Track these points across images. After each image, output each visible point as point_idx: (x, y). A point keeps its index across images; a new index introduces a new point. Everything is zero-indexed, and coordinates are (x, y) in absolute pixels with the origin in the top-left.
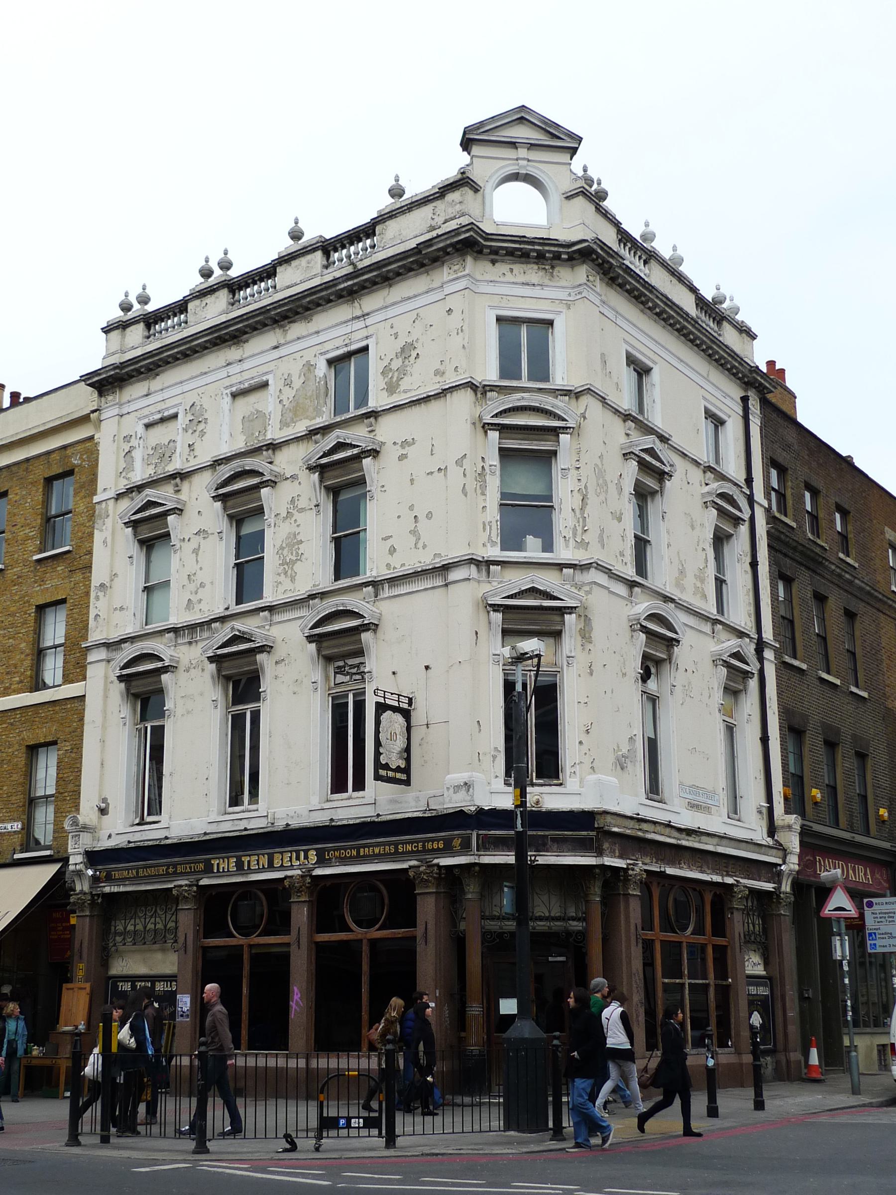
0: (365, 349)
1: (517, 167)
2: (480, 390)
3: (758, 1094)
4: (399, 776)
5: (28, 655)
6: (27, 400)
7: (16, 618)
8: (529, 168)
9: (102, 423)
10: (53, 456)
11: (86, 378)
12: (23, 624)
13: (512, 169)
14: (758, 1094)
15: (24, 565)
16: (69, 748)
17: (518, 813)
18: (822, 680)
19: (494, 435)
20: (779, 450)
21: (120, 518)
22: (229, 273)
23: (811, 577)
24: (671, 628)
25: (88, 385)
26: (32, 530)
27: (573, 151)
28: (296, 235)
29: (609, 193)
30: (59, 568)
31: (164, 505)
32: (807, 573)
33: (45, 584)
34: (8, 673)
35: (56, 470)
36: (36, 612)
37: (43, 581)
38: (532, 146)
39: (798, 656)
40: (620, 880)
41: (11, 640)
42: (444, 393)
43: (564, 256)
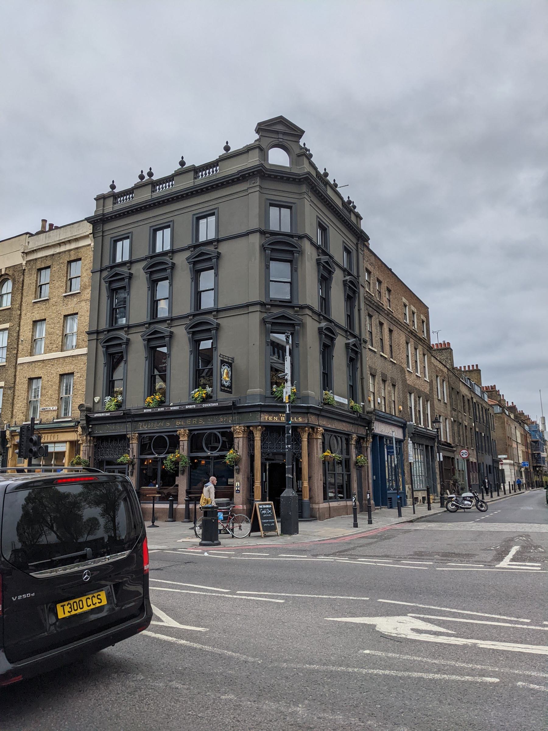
3: (370, 517)
4: (228, 389)
5: (60, 336)
6: (57, 228)
11: (87, 219)
13: (276, 142)
14: (370, 517)
17: (288, 406)
18: (381, 356)
20: (369, 265)
22: (114, 190)
23: (378, 315)
24: (334, 334)
27: (300, 136)
28: (182, 163)
31: (123, 275)
32: (377, 314)
34: (51, 343)
35: (72, 258)
36: (64, 318)
38: (284, 134)
39: (374, 346)
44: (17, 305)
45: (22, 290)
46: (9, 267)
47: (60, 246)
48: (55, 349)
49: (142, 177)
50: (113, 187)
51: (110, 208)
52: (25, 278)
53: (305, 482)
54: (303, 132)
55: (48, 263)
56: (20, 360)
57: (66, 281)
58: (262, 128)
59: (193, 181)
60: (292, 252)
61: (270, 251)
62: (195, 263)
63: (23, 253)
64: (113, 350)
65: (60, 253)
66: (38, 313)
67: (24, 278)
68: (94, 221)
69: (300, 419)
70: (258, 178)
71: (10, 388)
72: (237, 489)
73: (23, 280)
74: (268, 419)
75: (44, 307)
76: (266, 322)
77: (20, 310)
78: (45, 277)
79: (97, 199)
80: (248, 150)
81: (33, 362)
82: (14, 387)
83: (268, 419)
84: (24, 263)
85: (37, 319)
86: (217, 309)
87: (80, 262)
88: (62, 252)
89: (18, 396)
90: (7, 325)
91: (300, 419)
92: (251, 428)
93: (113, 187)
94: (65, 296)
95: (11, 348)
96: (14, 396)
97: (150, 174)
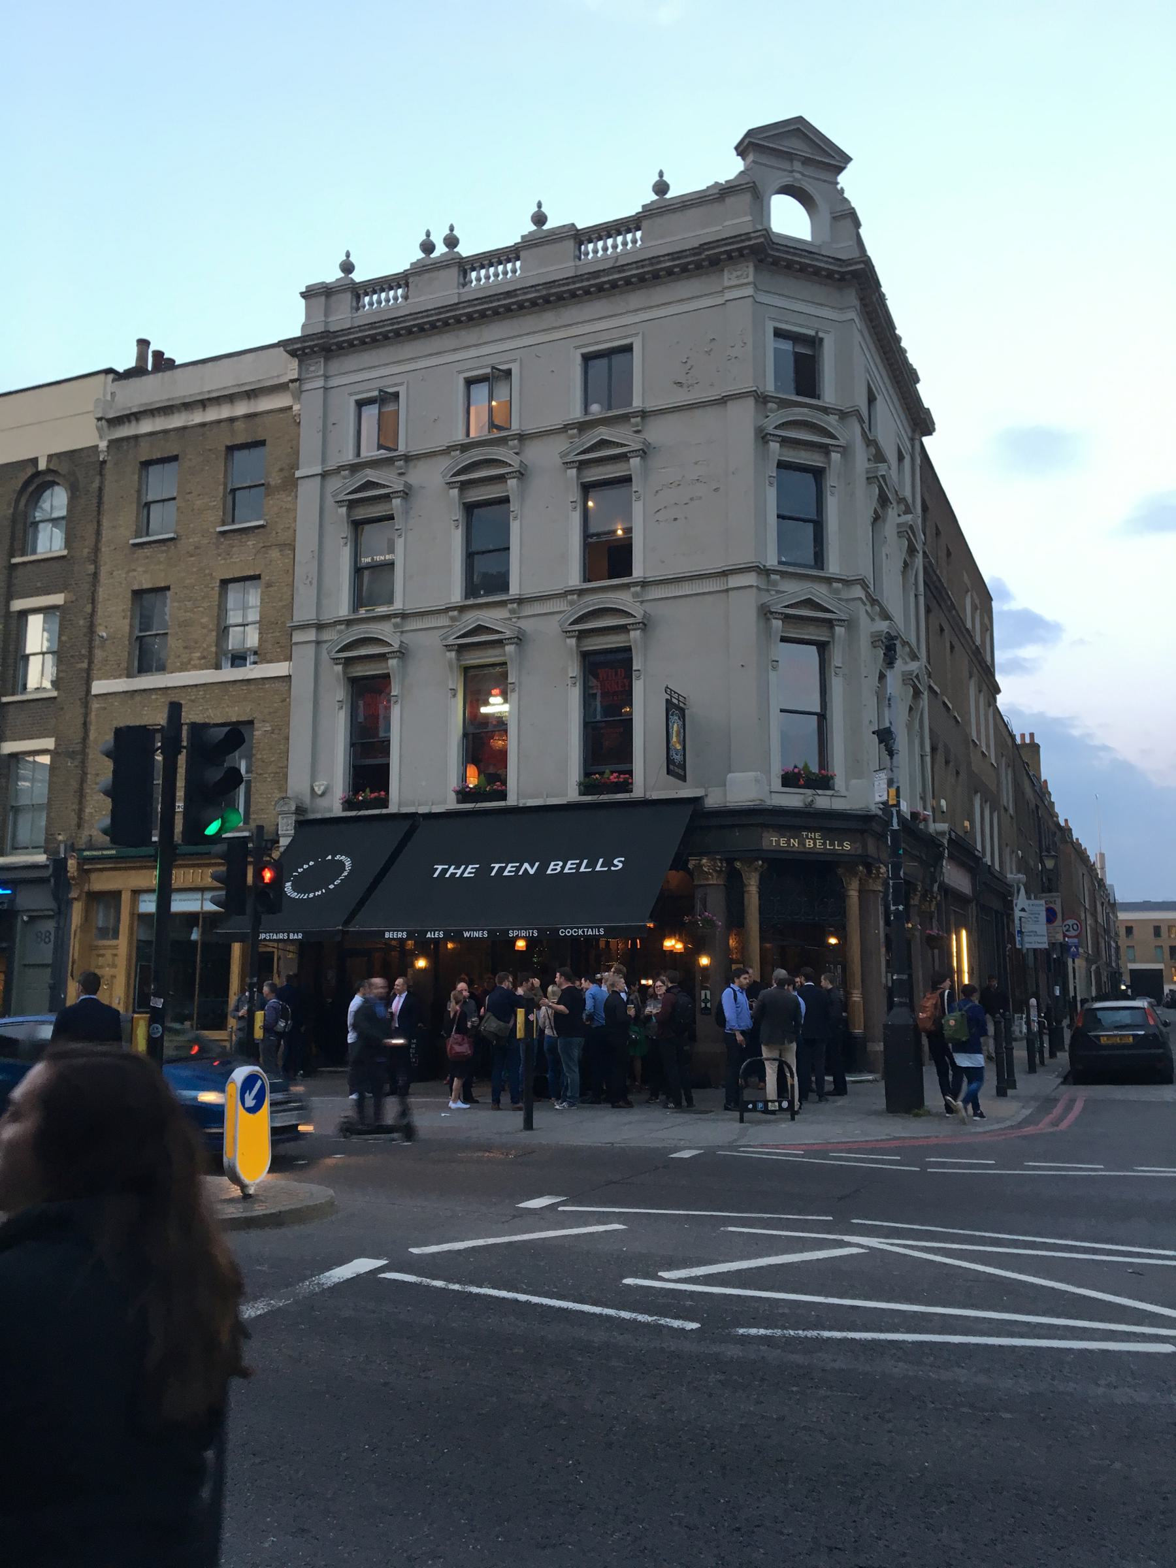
0: (628, 349)
1: (792, 179)
2: (762, 399)
7: (195, 591)
8: (802, 182)
9: (304, 393)
10: (237, 424)
12: (204, 598)
15: (203, 536)
16: (269, 729)
19: (774, 446)
21: (333, 496)
25: (287, 351)
26: (213, 499)
27: (840, 169)
29: (460, 241)
30: (249, 543)
31: (388, 487)
33: (231, 558)
34: (186, 648)
36: (220, 586)
37: (229, 554)
38: (807, 161)
40: (871, 877)
41: (188, 614)
42: (723, 401)
43: (836, 276)
44: (86, 551)
45: (99, 513)
46: (58, 455)
47: (137, 420)
48: (197, 662)
49: (428, 247)
50: (347, 267)
51: (342, 317)
52: (106, 483)
53: (856, 991)
54: (848, 159)
55: (172, 449)
56: (98, 687)
57: (225, 496)
58: (750, 145)
59: (323, 319)
60: (825, 450)
61: (778, 445)
62: (352, 505)
63: (99, 419)
64: (360, 671)
65: (203, 425)
66: (145, 572)
67: (102, 483)
68: (303, 349)
69: (847, 846)
70: (751, 265)
71: (71, 755)
72: (703, 1005)
73: (100, 489)
74: (778, 842)
75: (162, 557)
76: (772, 613)
77: (95, 562)
78: (161, 483)
79: (309, 294)
80: (722, 193)
81: (136, 691)
82: (83, 752)
83: (778, 842)
84: (103, 445)
85: (145, 586)
86: (645, 578)
87: (174, 465)
88: (212, 423)
89: (97, 775)
90: (58, 599)
91: (847, 846)
92: (738, 865)
93: (347, 267)
94: (135, 545)
95: (72, 656)
96: (85, 774)
97: (451, 241)
